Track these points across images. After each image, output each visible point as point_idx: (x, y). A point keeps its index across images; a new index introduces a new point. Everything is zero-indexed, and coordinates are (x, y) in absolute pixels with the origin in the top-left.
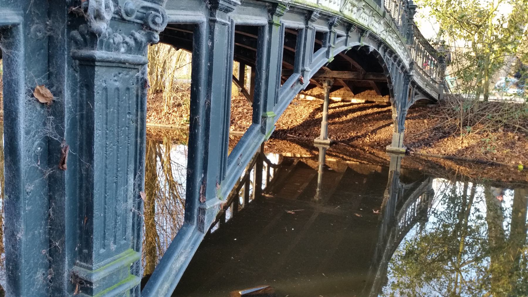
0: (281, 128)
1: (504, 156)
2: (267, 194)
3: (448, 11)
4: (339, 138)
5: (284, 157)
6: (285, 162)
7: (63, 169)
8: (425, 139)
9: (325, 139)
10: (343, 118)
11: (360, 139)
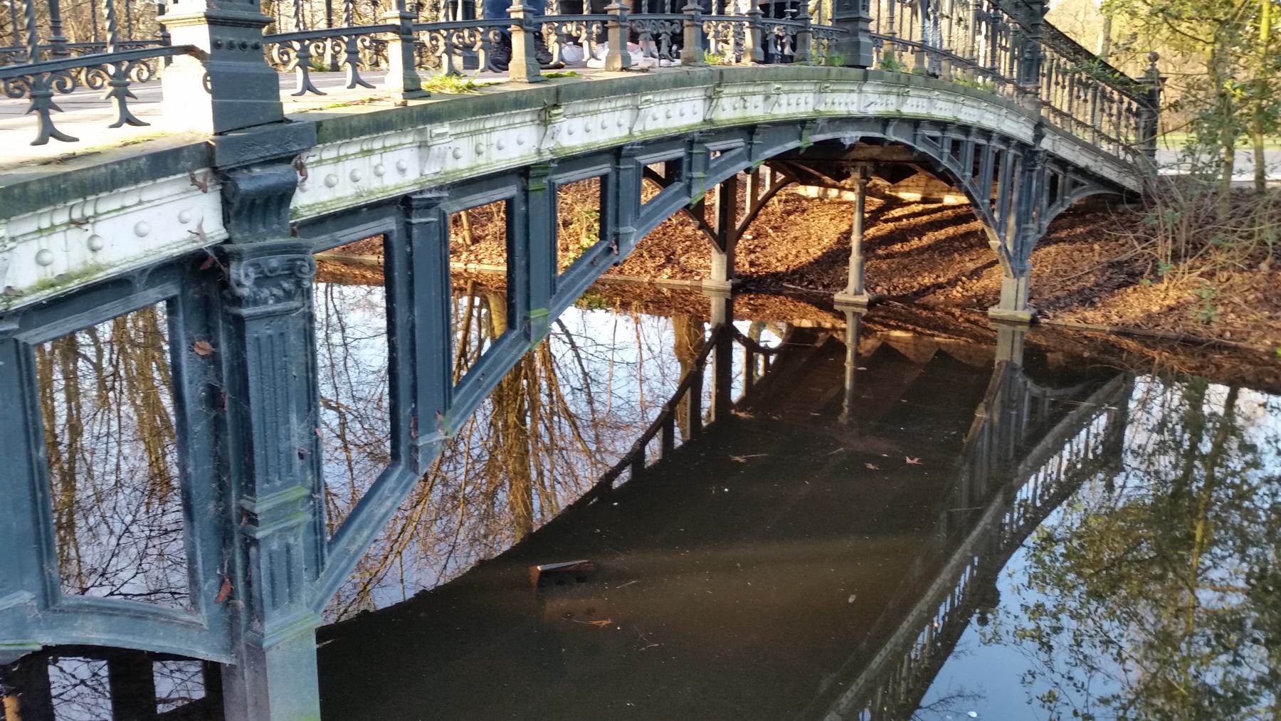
0: (771, 270)
1: (1249, 329)
2: (741, 411)
3: (1089, 22)
4: (895, 289)
5: (796, 328)
6: (796, 337)
7: (224, 412)
8: (1084, 288)
9: (857, 293)
10: (913, 242)
11: (941, 291)
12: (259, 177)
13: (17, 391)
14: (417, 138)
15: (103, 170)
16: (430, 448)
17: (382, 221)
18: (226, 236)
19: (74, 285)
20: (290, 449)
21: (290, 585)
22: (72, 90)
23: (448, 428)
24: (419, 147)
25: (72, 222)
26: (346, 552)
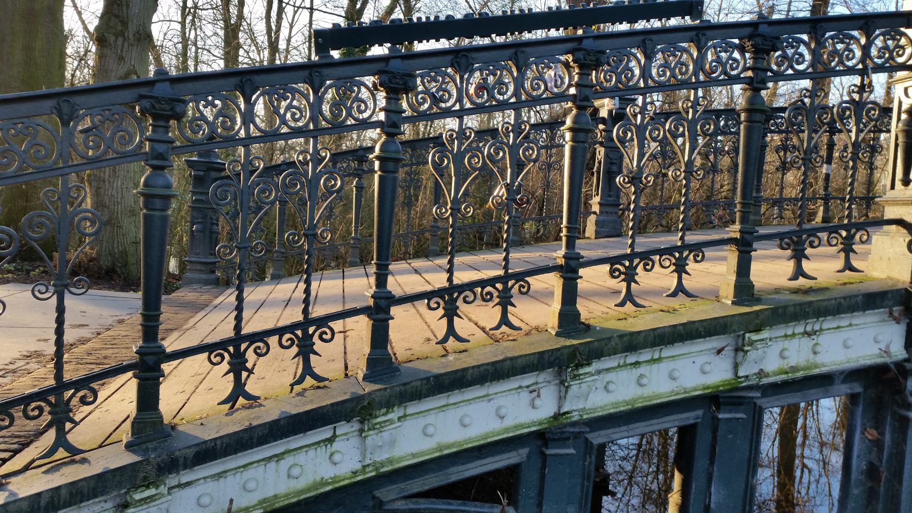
7: (880, 485)
15: (833, 302)
18: (906, 356)
19: (800, 374)
22: (818, 246)
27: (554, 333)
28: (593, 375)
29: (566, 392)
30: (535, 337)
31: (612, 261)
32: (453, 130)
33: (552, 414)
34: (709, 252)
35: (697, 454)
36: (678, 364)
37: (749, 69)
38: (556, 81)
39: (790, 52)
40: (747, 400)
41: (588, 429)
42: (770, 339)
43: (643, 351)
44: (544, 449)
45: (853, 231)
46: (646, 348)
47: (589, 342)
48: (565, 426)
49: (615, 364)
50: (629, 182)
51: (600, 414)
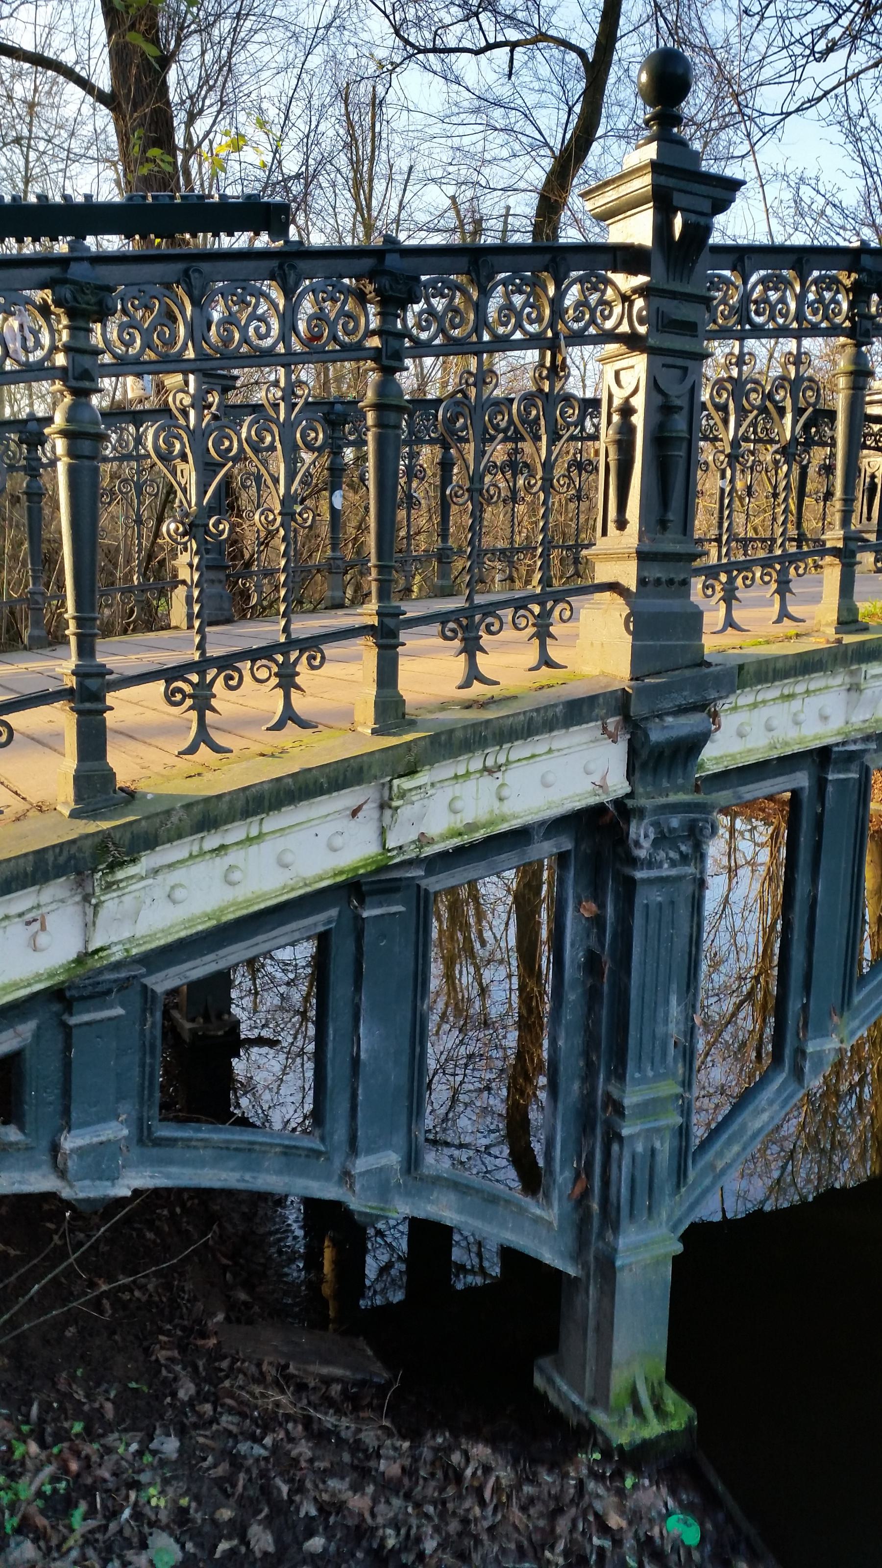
12: (671, 727)
13: (413, 938)
14: (848, 680)
15: (522, 717)
16: (820, 1056)
17: (793, 776)
18: (628, 790)
19: (480, 835)
20: (667, 1036)
21: (650, 1198)
23: (845, 1033)
24: (849, 690)
25: (485, 769)
26: (712, 1166)
27: (67, 813)
28: (142, 878)
29: (95, 914)
30: (34, 821)
31: (170, 674)
32: (790, 353)
33: (73, 956)
34: (330, 650)
35: (332, 978)
36: (289, 841)
37: (373, 333)
38: (24, 339)
39: (439, 304)
40: (404, 883)
41: (143, 970)
42: (433, 785)
43: (229, 826)
44: (65, 1017)
45: (549, 605)
46: (233, 821)
47: (131, 823)
48: (100, 971)
49: (185, 854)
50: (184, 535)
51: (162, 942)
